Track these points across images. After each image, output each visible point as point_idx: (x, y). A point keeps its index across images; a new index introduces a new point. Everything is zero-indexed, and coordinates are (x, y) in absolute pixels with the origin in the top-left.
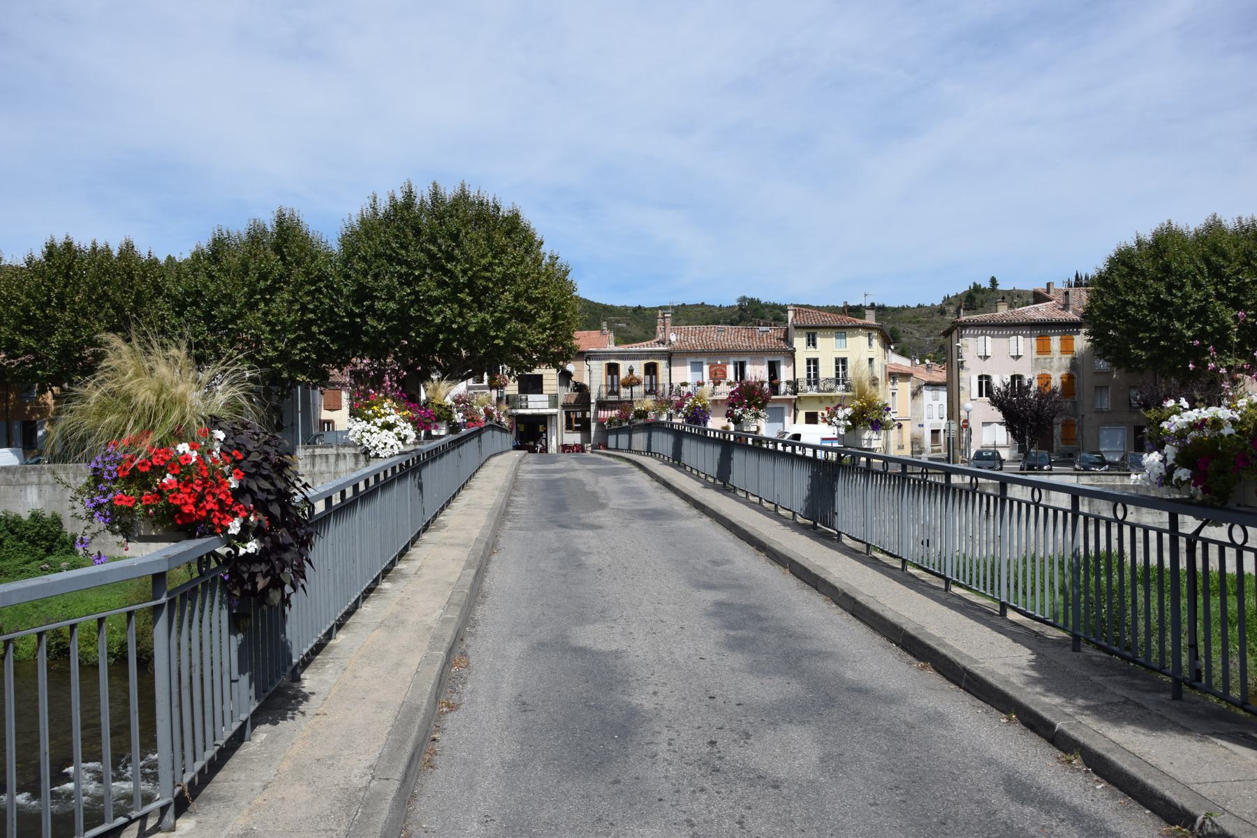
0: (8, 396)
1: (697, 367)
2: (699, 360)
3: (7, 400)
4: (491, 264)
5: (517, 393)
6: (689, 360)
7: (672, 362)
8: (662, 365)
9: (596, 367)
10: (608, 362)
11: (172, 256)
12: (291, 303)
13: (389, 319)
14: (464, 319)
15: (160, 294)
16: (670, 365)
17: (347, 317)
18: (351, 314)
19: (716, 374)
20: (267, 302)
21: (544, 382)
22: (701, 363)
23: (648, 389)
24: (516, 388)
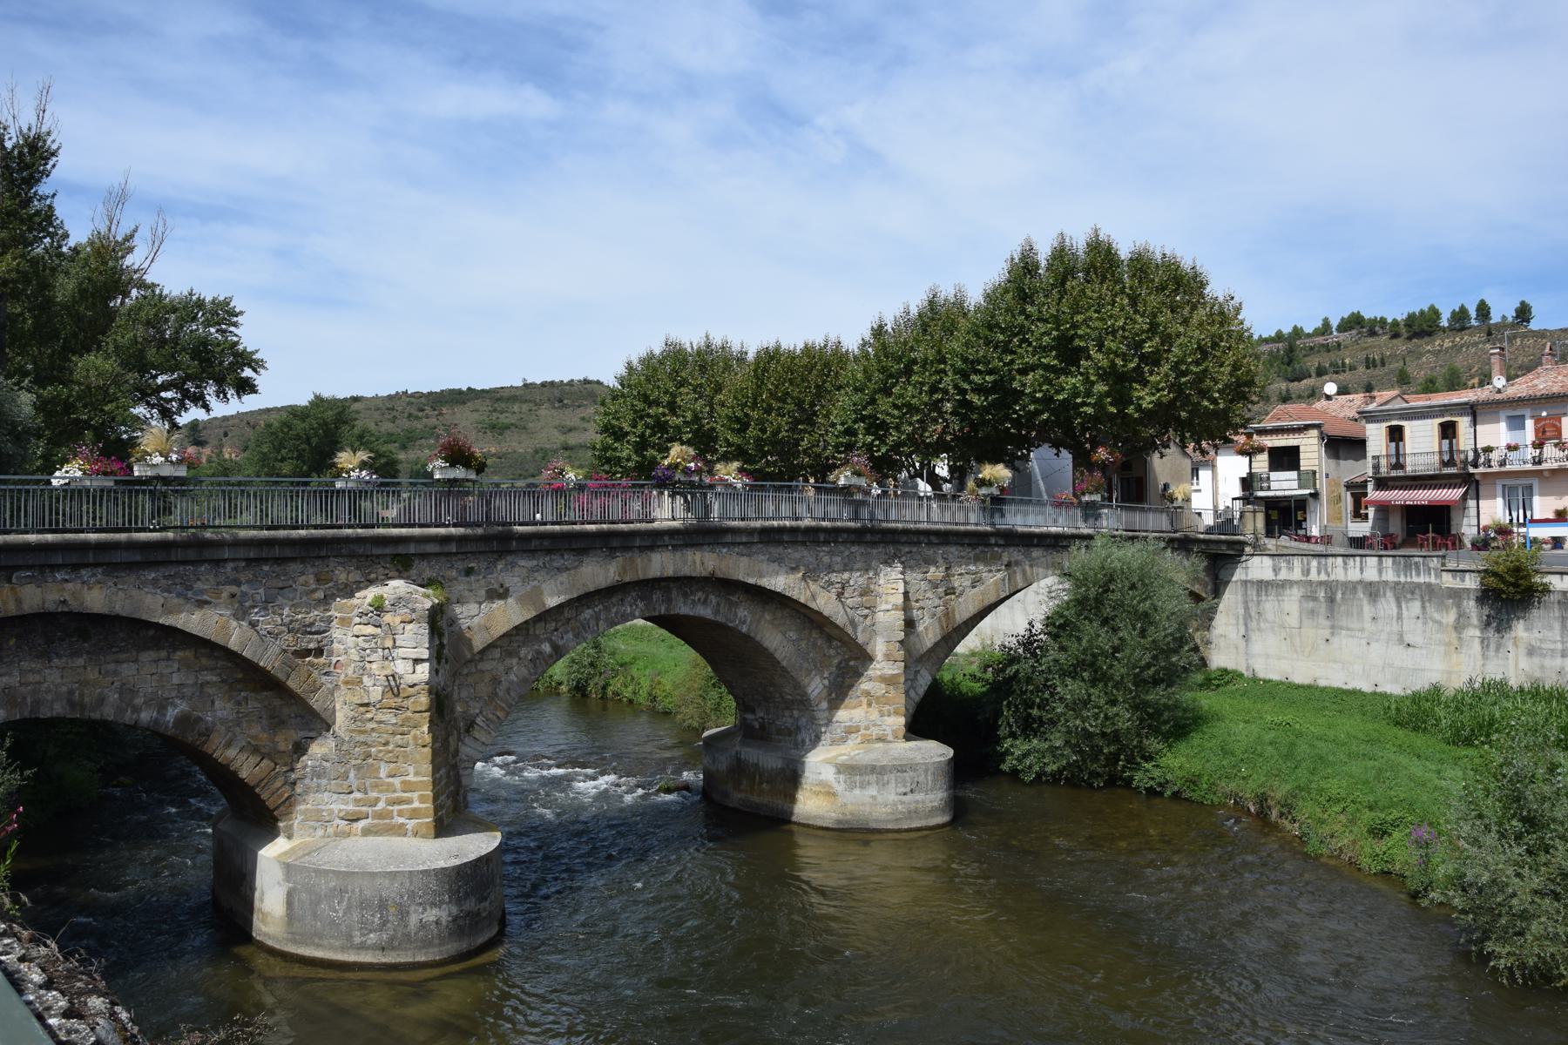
1: (1516, 423)
2: (1518, 412)
5: (1267, 470)
6: (1503, 414)
7: (1478, 418)
8: (1463, 423)
9: (1375, 432)
10: (1389, 424)
11: (1299, 327)
16: (1475, 423)
19: (1544, 432)
21: (1302, 456)
22: (1523, 417)
23: (1446, 458)
24: (1266, 464)
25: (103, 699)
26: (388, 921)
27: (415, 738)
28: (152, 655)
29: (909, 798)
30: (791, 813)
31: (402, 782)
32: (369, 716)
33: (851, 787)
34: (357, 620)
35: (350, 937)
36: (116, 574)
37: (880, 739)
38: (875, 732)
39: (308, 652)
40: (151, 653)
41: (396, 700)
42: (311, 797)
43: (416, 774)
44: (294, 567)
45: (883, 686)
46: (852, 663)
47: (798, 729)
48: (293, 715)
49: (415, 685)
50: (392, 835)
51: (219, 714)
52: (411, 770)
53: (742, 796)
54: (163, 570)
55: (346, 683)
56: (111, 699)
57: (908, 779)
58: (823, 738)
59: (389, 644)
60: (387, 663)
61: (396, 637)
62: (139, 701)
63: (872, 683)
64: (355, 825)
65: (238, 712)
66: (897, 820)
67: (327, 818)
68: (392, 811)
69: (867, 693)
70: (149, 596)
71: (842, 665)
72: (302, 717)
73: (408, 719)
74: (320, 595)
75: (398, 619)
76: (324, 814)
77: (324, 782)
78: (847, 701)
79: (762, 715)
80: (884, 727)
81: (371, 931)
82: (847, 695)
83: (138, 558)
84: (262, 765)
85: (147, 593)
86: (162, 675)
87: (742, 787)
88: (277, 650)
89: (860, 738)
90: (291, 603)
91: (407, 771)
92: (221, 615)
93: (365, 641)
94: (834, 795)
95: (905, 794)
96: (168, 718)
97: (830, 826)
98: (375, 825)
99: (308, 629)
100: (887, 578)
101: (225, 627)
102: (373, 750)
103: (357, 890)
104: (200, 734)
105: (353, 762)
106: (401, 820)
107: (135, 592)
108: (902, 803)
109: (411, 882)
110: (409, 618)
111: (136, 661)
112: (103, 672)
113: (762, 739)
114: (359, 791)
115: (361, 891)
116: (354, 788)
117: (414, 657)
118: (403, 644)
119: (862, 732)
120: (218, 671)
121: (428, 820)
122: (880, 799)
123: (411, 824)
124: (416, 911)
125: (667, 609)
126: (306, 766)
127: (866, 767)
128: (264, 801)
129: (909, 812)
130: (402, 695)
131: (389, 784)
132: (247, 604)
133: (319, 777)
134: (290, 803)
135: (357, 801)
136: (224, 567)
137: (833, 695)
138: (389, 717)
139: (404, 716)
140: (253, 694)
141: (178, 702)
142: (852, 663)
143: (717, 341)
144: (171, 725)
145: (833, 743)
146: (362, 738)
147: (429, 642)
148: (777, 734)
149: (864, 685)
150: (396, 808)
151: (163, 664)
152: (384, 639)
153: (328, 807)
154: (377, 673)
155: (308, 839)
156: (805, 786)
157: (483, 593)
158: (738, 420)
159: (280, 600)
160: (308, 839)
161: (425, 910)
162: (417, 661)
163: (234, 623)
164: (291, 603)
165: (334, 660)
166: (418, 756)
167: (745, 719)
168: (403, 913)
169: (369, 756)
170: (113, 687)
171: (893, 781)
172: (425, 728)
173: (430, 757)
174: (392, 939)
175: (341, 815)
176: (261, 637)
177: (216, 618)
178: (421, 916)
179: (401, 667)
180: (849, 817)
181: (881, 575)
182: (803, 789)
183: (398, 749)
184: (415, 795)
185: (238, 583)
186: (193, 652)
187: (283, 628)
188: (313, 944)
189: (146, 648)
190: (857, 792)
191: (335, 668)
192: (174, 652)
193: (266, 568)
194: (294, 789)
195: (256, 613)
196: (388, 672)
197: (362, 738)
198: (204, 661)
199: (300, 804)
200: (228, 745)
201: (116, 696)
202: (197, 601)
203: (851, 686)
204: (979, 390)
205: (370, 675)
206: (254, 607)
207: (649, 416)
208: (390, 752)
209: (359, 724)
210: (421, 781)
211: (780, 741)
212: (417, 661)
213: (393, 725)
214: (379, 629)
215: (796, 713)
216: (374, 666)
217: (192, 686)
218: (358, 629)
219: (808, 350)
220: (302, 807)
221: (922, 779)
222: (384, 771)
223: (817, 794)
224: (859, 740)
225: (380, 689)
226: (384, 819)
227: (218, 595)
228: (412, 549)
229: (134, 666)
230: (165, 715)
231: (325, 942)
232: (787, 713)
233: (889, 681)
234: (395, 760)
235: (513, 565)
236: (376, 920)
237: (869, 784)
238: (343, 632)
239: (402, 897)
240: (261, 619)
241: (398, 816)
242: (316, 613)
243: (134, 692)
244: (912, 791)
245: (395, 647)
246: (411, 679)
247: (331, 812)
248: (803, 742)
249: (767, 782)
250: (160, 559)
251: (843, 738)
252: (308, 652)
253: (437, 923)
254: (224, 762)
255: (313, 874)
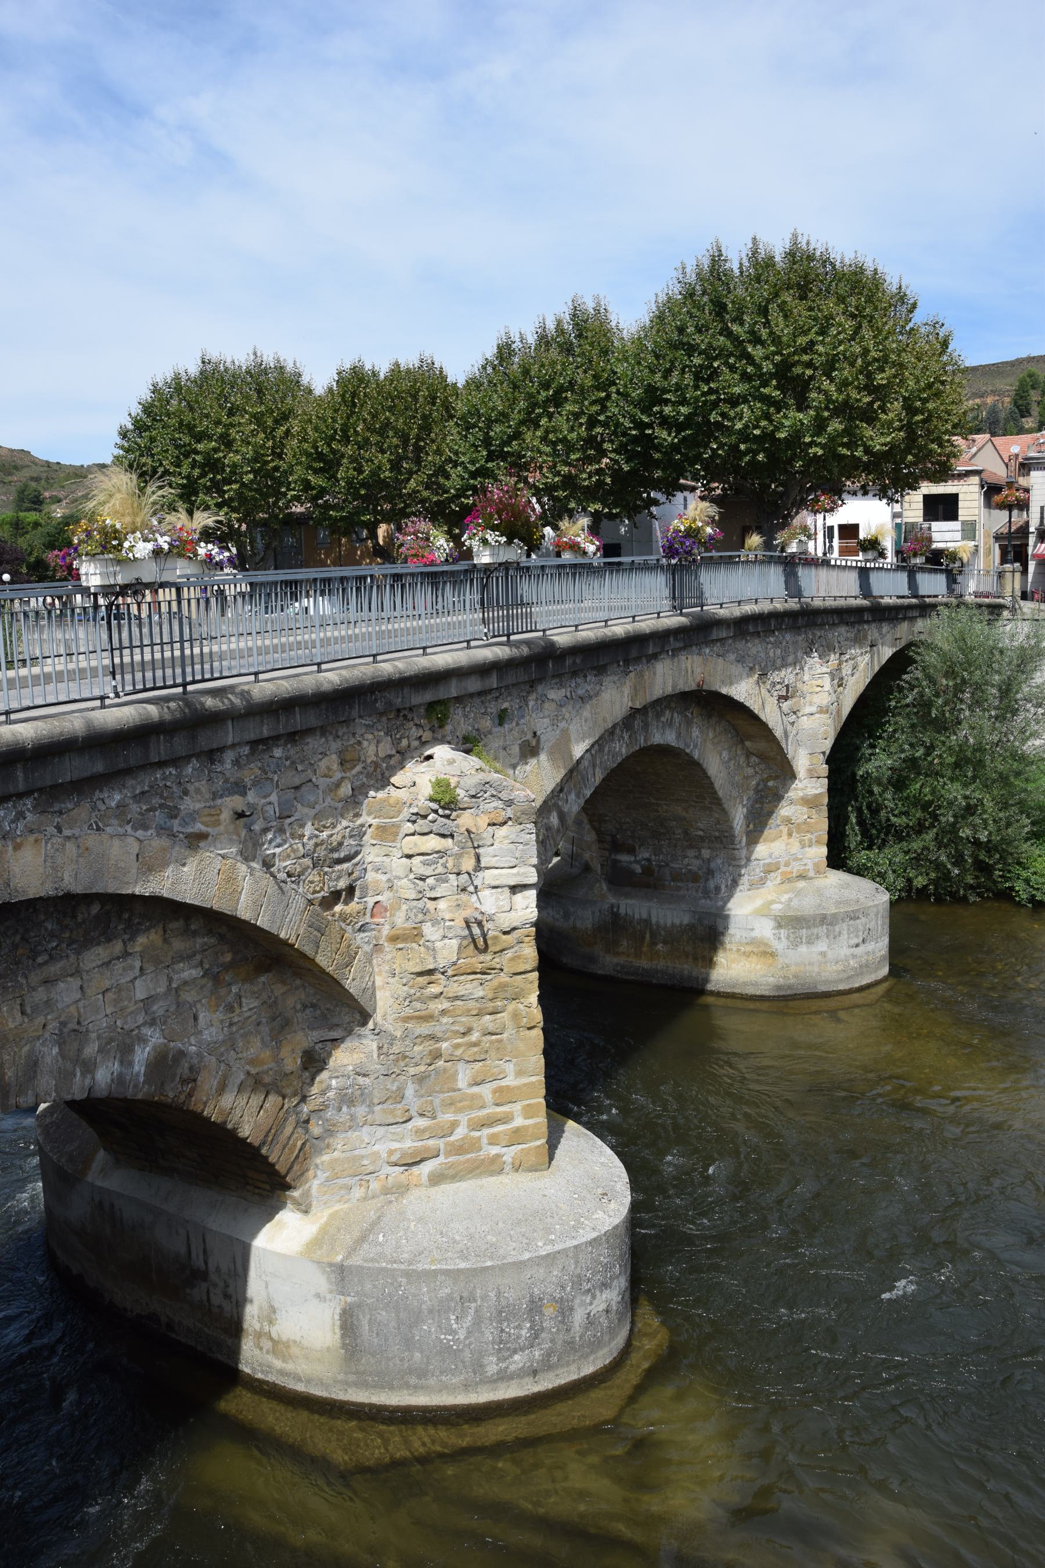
0: (340, 540)
3: (340, 545)
4: (812, 343)
5: (921, 519)
12: (577, 416)
13: (680, 427)
14: (771, 421)
15: (452, 417)
17: (634, 428)
18: (640, 425)
20: (550, 416)
21: (961, 504)
25: (36, 1064)
26: (543, 1329)
27: (516, 1016)
28: (97, 954)
29: (861, 949)
30: (706, 980)
31: (495, 1092)
32: (434, 989)
33: (795, 944)
34: (409, 827)
35: (478, 1366)
36: (57, 807)
37: (802, 877)
38: (796, 868)
39: (335, 897)
40: (100, 950)
41: (482, 958)
42: (338, 1142)
43: (519, 1073)
44: (314, 743)
45: (805, 809)
46: (771, 784)
47: (710, 873)
48: (299, 1007)
49: (514, 929)
50: (480, 1175)
51: (206, 1036)
52: (510, 1068)
53: (621, 960)
54: (130, 782)
55: (394, 939)
56: (48, 1060)
57: (860, 927)
58: (741, 882)
59: (468, 864)
60: (464, 896)
61: (481, 851)
62: (91, 1049)
63: (793, 807)
64: (415, 1170)
65: (231, 1025)
66: (848, 978)
67: (371, 1168)
68: (480, 1138)
69: (788, 821)
70: (116, 842)
71: (760, 788)
72: (314, 1006)
73: (503, 986)
74: (346, 790)
75: (483, 821)
76: (365, 1162)
77: (361, 1110)
78: (766, 832)
79: (646, 855)
80: (805, 861)
81: (515, 1352)
82: (766, 824)
83: (99, 767)
84: (267, 1105)
85: (112, 837)
86: (119, 989)
87: (621, 949)
88: (301, 903)
89: (779, 878)
90: (312, 812)
91: (503, 1071)
92: (223, 857)
93: (424, 863)
94: (773, 955)
95: (857, 946)
96: (137, 1068)
97: (767, 993)
98: (452, 1166)
99: (336, 855)
100: (812, 672)
101: (231, 879)
102: (444, 1045)
103: (492, 1295)
104: (184, 1081)
105: (412, 1071)
106: (494, 1150)
107: (92, 840)
108: (854, 956)
109: (577, 1262)
110: (502, 816)
111: (77, 972)
112: (29, 1010)
113: (648, 886)
114: (422, 1115)
115: (499, 1294)
116: (413, 1113)
117: (513, 883)
118: (493, 862)
119: (783, 869)
120: (198, 957)
121: (539, 1143)
122: (830, 955)
123: (509, 1154)
124: (583, 1304)
125: (645, 740)
126: (329, 1088)
127: (814, 917)
128: (273, 1165)
129: (861, 966)
130: (492, 949)
131: (473, 1097)
132: (257, 827)
133: (351, 1102)
134: (303, 1156)
135: (419, 1132)
136: (222, 762)
137: (751, 826)
138: (472, 988)
139: (495, 983)
140: (247, 986)
141: (147, 1031)
142: (771, 784)
143: (269, 360)
144: (142, 1079)
145: (752, 886)
146: (424, 1029)
147: (539, 856)
148: (673, 880)
149: (785, 810)
150: (486, 1132)
151: (119, 966)
152: (459, 856)
153: (370, 1150)
154: (447, 917)
155: (337, 1207)
156: (728, 946)
157: (516, 749)
158: (320, 456)
159: (301, 810)
160: (337, 1207)
161: (594, 1297)
162: (515, 889)
163: (243, 868)
164: (312, 812)
165: (370, 901)
166: (521, 1046)
167: (615, 861)
168: (565, 1310)
169: (437, 1055)
170: (47, 1035)
171: (845, 932)
172: (533, 998)
173: (541, 1044)
174: (549, 1354)
175: (394, 1158)
176: (280, 884)
177: (218, 863)
178: (589, 1308)
179: (490, 902)
180: (792, 981)
181: (806, 669)
182: (725, 949)
183: (489, 1037)
184: (517, 1107)
185: (240, 789)
186: (160, 932)
187: (307, 861)
188: (407, 1386)
189: (87, 943)
190: (803, 949)
191: (372, 916)
192: (132, 939)
193: (278, 752)
194: (307, 1131)
195: (270, 842)
196: (468, 913)
197: (424, 1029)
198: (178, 944)
199: (319, 1152)
200: (222, 1089)
201: (55, 1051)
202: (188, 836)
203: (770, 813)
204: (665, 422)
205: (435, 922)
206: (265, 830)
207: (197, 453)
208: (475, 1044)
209: (418, 1005)
210: (525, 1085)
211: (679, 888)
212: (515, 889)
213: (477, 1000)
214: (450, 840)
215: (706, 853)
216: (442, 905)
217: (166, 994)
218: (410, 844)
219: (396, 371)
220: (326, 1158)
221: (872, 925)
222: (463, 1076)
223: (747, 955)
224: (778, 881)
225: (455, 943)
226: (467, 1152)
227: (214, 814)
228: (453, 689)
229: (75, 983)
230: (131, 1064)
231: (432, 1381)
232: (691, 853)
233: (810, 802)
234: (483, 1057)
235: (543, 699)
236: (524, 1332)
237: (818, 937)
238: (384, 850)
239: (563, 1288)
240: (278, 850)
241: (490, 1144)
242: (345, 823)
243: (79, 1034)
244: (864, 941)
245: (478, 868)
246: (506, 921)
247: (376, 1155)
248: (718, 889)
249: (665, 942)
250: (132, 762)
251: (761, 879)
252: (335, 897)
253: (607, 1311)
254: (219, 1121)
255: (404, 1280)
